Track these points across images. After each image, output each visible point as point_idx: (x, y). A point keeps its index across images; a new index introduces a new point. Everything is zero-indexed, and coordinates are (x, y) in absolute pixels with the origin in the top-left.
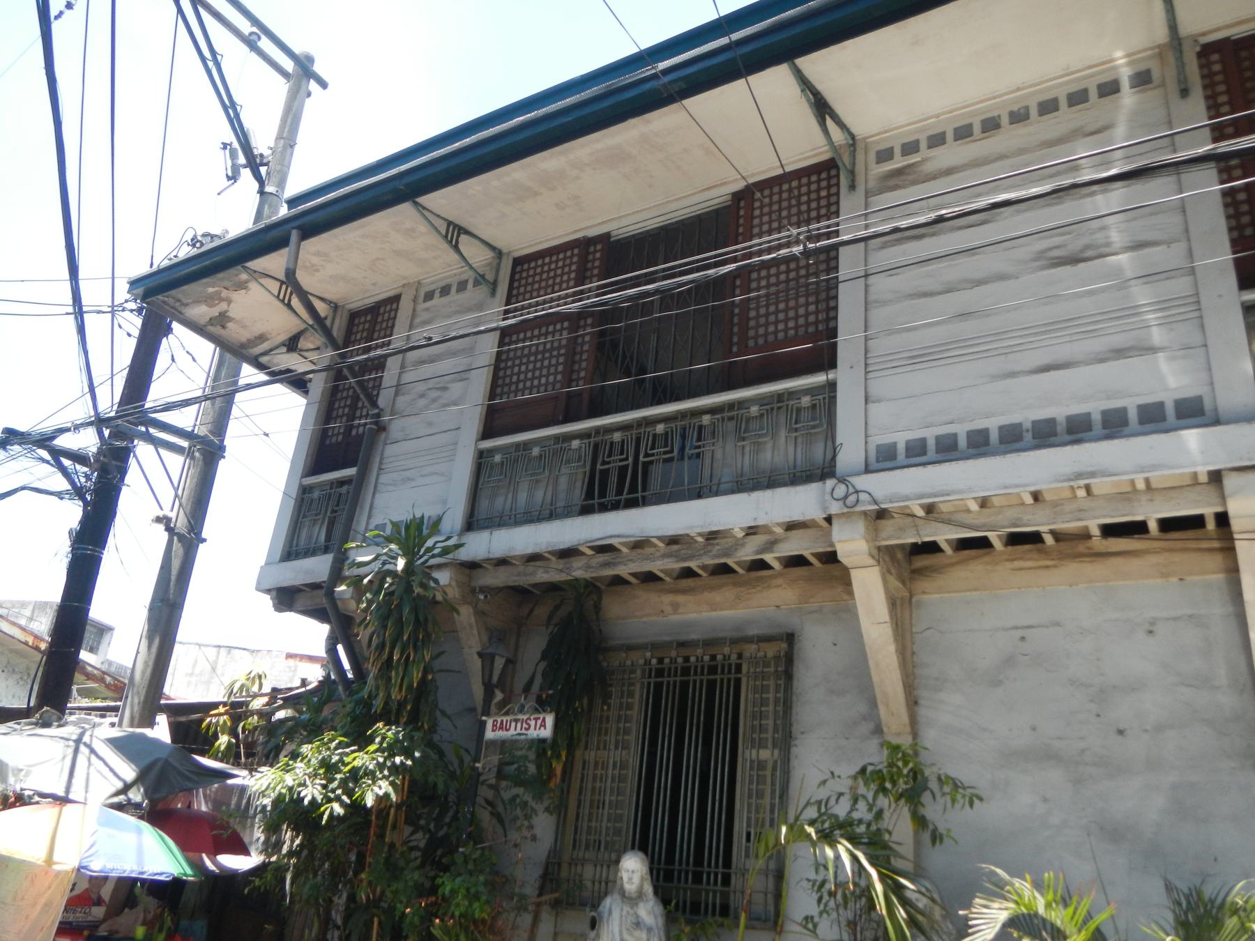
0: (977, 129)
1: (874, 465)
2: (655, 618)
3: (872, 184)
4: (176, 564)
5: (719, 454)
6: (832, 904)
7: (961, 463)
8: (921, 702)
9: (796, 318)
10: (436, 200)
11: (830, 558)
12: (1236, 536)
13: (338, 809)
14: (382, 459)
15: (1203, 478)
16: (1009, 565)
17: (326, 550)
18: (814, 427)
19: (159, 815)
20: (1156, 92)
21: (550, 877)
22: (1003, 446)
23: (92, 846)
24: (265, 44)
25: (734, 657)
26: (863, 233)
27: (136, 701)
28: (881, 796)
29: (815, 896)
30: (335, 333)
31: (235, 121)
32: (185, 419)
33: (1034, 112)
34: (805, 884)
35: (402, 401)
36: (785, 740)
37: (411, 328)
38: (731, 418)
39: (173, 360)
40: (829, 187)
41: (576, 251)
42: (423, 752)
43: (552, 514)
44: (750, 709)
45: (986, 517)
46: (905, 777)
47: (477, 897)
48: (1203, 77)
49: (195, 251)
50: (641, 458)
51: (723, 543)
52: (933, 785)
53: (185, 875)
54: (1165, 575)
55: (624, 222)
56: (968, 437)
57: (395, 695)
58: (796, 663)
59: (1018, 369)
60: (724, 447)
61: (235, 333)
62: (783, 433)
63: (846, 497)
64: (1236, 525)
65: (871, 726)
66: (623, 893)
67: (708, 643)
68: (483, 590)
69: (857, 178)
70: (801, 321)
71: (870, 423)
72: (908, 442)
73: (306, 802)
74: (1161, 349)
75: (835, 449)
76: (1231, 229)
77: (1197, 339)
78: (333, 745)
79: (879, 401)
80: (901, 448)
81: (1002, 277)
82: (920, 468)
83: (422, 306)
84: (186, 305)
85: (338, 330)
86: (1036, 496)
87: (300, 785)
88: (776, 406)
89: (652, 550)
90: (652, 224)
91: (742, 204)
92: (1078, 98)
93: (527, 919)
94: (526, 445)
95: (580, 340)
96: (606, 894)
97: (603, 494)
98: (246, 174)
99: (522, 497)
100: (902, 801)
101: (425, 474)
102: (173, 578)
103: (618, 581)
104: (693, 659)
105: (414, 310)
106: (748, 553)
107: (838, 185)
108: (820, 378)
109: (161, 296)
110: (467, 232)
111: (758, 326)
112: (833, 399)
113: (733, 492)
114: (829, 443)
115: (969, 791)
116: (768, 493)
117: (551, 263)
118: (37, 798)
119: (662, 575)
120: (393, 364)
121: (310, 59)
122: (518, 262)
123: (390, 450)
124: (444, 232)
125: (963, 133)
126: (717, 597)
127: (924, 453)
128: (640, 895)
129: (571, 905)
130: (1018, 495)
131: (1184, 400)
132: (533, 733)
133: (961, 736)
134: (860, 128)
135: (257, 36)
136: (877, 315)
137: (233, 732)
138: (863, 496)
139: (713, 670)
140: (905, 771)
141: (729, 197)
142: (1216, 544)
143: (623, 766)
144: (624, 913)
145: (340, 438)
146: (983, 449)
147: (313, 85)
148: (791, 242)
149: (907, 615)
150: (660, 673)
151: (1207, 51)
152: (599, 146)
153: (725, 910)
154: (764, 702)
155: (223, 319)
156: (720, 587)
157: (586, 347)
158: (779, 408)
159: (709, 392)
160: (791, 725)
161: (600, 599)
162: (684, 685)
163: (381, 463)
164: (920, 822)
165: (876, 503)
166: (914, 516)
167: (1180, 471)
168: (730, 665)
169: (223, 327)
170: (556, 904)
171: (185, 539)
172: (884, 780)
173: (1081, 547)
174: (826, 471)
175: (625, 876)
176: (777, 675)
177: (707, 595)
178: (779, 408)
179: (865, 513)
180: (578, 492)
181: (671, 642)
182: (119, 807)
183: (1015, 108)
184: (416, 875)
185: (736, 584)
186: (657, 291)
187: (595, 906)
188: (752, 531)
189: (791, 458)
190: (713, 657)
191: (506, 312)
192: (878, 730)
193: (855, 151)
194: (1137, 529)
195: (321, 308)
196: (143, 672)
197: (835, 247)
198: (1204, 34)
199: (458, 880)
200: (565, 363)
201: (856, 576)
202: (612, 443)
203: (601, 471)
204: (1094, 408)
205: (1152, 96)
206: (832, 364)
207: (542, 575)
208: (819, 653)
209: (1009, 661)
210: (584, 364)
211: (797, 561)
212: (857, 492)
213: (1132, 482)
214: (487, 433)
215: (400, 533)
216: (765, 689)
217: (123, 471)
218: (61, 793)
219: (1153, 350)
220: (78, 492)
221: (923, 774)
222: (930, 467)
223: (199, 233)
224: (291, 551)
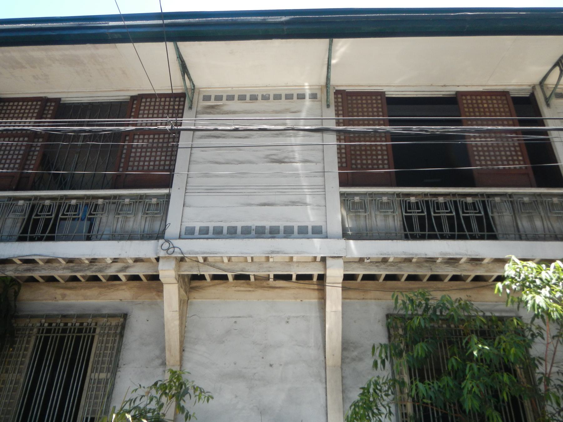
1: (183, 236)
2: (50, 301)
5: (104, 219)
7: (224, 240)
8: (186, 349)
9: (155, 161)
11: (155, 278)
12: (327, 284)
15: (318, 259)
18: (156, 214)
20: (318, 103)
25: (93, 324)
26: (193, 127)
28: (164, 396)
38: (114, 203)
48: (335, 102)
50: (60, 216)
51: (99, 265)
52: (191, 391)
54: (296, 298)
55: (70, 95)
58: (126, 329)
59: (253, 203)
60: (108, 217)
62: (140, 214)
63: (168, 249)
64: (328, 280)
65: (160, 361)
67: (79, 316)
69: (193, 104)
70: (157, 163)
71: (184, 215)
72: (200, 228)
74: (310, 205)
75: (166, 226)
76: (339, 163)
77: (323, 203)
79: (190, 206)
80: (197, 229)
81: (250, 162)
82: (205, 240)
86: (205, 259)
88: (138, 201)
89: (57, 265)
90: (86, 100)
91: (135, 102)
92: (289, 97)
97: (33, 231)
103: (32, 280)
104: (69, 324)
106: (111, 272)
107: (184, 105)
108: (165, 191)
111: (134, 161)
112: (168, 203)
113: (109, 240)
114: (163, 223)
115: (208, 394)
116: (128, 243)
125: (242, 98)
126: (89, 292)
127: (207, 233)
130: (197, 257)
131: (316, 226)
133: (201, 369)
134: (198, 83)
136: (193, 167)
138: (176, 250)
139: (80, 331)
141: (129, 97)
142: (316, 287)
143: (17, 383)
146: (233, 235)
148: (164, 124)
149: (185, 308)
150: (49, 331)
151: (337, 92)
152: (67, 53)
156: (91, 287)
158: (140, 202)
159: (102, 188)
160: (119, 360)
161: (19, 289)
162: (62, 339)
164: (181, 409)
165: (182, 253)
167: (308, 255)
168: (90, 329)
173: (265, 284)
174: (159, 235)
176: (115, 334)
177: (83, 291)
178: (140, 202)
179: (176, 258)
180: (17, 229)
181: (58, 315)
185: (100, 287)
186: (90, 131)
188: (115, 260)
190: (82, 324)
192: (164, 364)
193: (194, 92)
194: (288, 278)
198: (337, 86)
200: (22, 159)
201: (166, 288)
202: (43, 206)
203: (34, 219)
204: (281, 224)
205: (317, 104)
208: (139, 324)
209: (228, 332)
210: (33, 162)
211: (136, 278)
212: (174, 247)
213: (246, 258)
219: (306, 204)
221: (185, 386)
222: (210, 240)
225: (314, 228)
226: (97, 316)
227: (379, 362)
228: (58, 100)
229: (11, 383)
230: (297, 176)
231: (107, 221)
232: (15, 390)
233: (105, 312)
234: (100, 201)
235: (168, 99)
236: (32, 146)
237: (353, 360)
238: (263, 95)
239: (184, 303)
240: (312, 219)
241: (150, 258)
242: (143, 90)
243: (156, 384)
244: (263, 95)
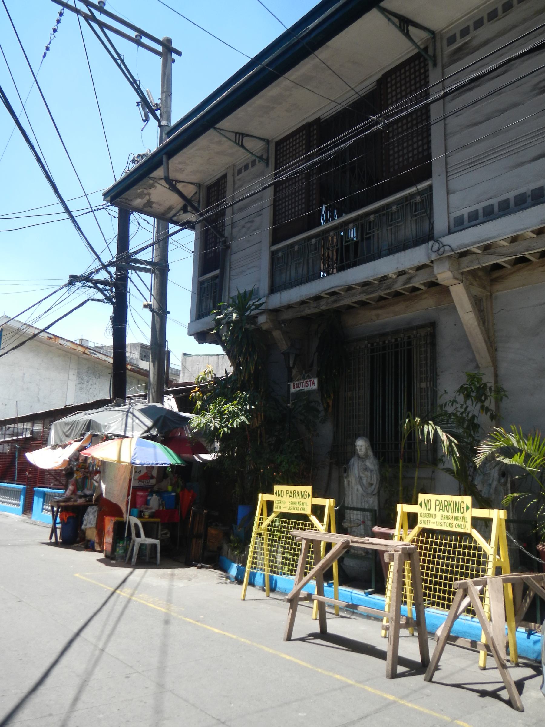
1: (453, 229)
4: (158, 326)
7: (494, 221)
10: (226, 124)
14: (230, 263)
23: (135, 454)
24: (144, 40)
27: (153, 391)
31: (138, 90)
32: (147, 255)
35: (235, 230)
37: (234, 191)
39: (139, 224)
41: (304, 132)
49: (135, 166)
50: (344, 244)
53: (177, 463)
55: (324, 111)
56: (454, 221)
63: (439, 249)
66: (359, 457)
67: (396, 332)
68: (283, 321)
72: (469, 213)
73: (212, 429)
78: (222, 403)
79: (454, 192)
81: (515, 105)
82: (474, 228)
83: (238, 177)
84: (131, 200)
94: (292, 245)
95: (311, 183)
96: (352, 457)
99: (293, 272)
102: (158, 333)
103: (349, 307)
105: (234, 181)
109: (123, 196)
110: (248, 135)
117: (405, 72)
118: (113, 437)
119: (386, 296)
120: (228, 212)
121: (169, 41)
122: (278, 144)
123: (234, 258)
124: (234, 141)
125: (493, 15)
127: (477, 218)
128: (366, 456)
132: (310, 388)
135: (139, 37)
138: (447, 248)
141: (376, 83)
144: (360, 465)
145: (212, 254)
147: (174, 56)
155: (149, 203)
157: (314, 187)
160: (436, 369)
163: (230, 265)
165: (453, 251)
166: (531, 238)
168: (404, 342)
171: (160, 313)
174: (427, 237)
175: (358, 448)
178: (407, 204)
179: (449, 257)
190: (396, 340)
191: (276, 174)
196: (154, 378)
203: (345, 246)
212: (444, 246)
214: (274, 242)
215: (235, 302)
220: (109, 299)
222: (479, 226)
223: (136, 156)
233: (415, 324)
234: (372, 217)
241: (368, 281)
242: (385, 68)
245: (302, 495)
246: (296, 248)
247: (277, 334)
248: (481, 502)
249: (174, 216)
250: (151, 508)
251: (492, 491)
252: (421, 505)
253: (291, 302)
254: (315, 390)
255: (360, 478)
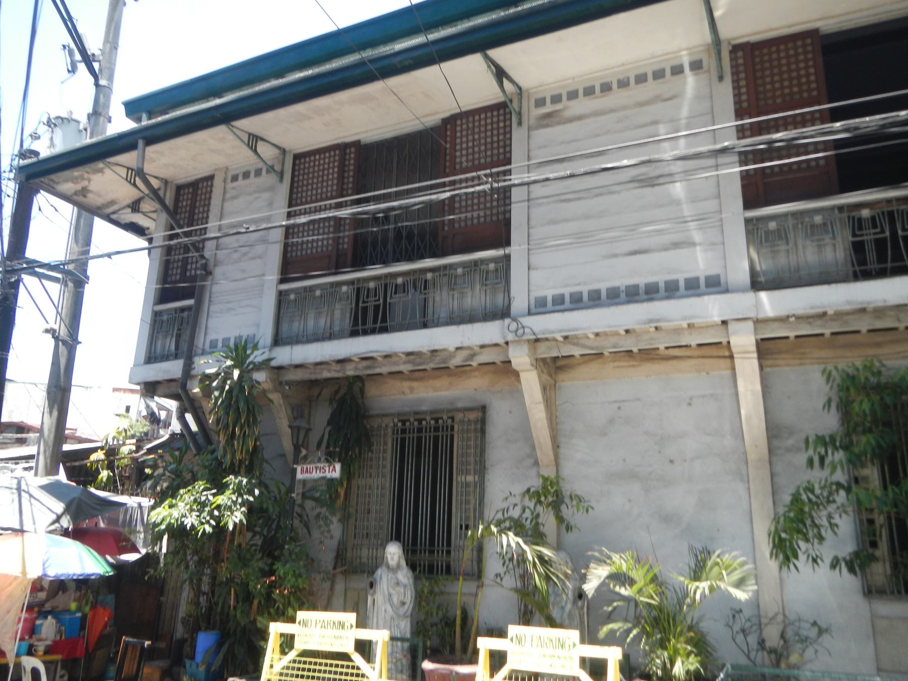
0: (598, 89)
1: (533, 310)
3: (532, 122)
4: (63, 361)
5: (438, 298)
6: (511, 566)
8: (561, 445)
13: (208, 529)
16: (612, 364)
17: (176, 357)
18: (497, 283)
19: (77, 534)
21: (340, 557)
22: (609, 301)
28: (538, 506)
29: (501, 562)
30: (167, 202)
33: (632, 81)
34: (495, 555)
36: (481, 469)
40: (505, 121)
42: (261, 492)
43: (330, 336)
44: (460, 451)
45: (599, 342)
46: (552, 494)
47: (300, 575)
52: (567, 500)
55: (370, 134)
57: (238, 456)
60: (441, 295)
61: (93, 199)
62: (478, 286)
63: (517, 330)
65: (532, 461)
66: (388, 566)
68: (288, 383)
79: (536, 269)
80: (549, 299)
83: (230, 185)
84: (58, 183)
85: (169, 200)
87: (183, 516)
89: (397, 359)
92: (659, 75)
93: (327, 585)
97: (364, 323)
98: (82, 67)
99: (311, 323)
100: (550, 508)
101: (242, 307)
102: (62, 371)
105: (225, 188)
106: (457, 361)
110: (262, 139)
122: (297, 157)
125: (589, 91)
128: (398, 566)
129: (355, 572)
133: (583, 470)
134: (524, 83)
137: (110, 466)
138: (527, 330)
140: (552, 491)
146: (597, 302)
150: (404, 431)
151: (736, 49)
153: (448, 570)
154: (468, 447)
155: (84, 191)
161: (364, 385)
163: (210, 297)
164: (560, 519)
165: (534, 334)
169: (85, 196)
170: (345, 573)
171: (67, 343)
172: (539, 497)
174: (504, 313)
179: (528, 341)
180: (347, 320)
182: (51, 532)
183: (621, 77)
184: (260, 564)
185: (450, 375)
186: (400, 208)
187: (372, 572)
189: (483, 303)
192: (536, 463)
195: (155, 183)
197: (510, 187)
198: (734, 39)
199: (288, 566)
204: (660, 279)
206: (508, 243)
207: (326, 374)
208: (501, 419)
209: (611, 421)
216: (469, 439)
217: (16, 297)
218: (18, 527)
219: (693, 244)
224: (152, 357)
225: (708, 279)
226: (452, 412)
227: (816, 459)
228: (357, 144)
229: (378, 489)
230: (678, 203)
231: (442, 300)
232: (383, 496)
233: (460, 405)
235: (489, 114)
236: (339, 237)
237: (788, 450)
238: (619, 81)
239: (549, 391)
240: (701, 264)
243: (528, 490)
244: (619, 81)
245: (342, 625)
246: (318, 293)
247: (275, 397)
248: (589, 637)
249: (114, 213)
250: (46, 640)
251: (565, 615)
252: (512, 640)
253: (307, 361)
254: (336, 479)
255: (390, 595)
